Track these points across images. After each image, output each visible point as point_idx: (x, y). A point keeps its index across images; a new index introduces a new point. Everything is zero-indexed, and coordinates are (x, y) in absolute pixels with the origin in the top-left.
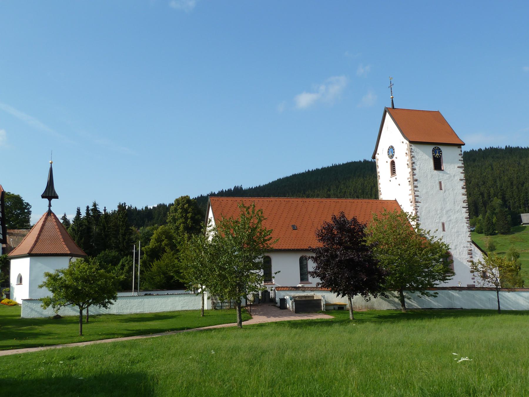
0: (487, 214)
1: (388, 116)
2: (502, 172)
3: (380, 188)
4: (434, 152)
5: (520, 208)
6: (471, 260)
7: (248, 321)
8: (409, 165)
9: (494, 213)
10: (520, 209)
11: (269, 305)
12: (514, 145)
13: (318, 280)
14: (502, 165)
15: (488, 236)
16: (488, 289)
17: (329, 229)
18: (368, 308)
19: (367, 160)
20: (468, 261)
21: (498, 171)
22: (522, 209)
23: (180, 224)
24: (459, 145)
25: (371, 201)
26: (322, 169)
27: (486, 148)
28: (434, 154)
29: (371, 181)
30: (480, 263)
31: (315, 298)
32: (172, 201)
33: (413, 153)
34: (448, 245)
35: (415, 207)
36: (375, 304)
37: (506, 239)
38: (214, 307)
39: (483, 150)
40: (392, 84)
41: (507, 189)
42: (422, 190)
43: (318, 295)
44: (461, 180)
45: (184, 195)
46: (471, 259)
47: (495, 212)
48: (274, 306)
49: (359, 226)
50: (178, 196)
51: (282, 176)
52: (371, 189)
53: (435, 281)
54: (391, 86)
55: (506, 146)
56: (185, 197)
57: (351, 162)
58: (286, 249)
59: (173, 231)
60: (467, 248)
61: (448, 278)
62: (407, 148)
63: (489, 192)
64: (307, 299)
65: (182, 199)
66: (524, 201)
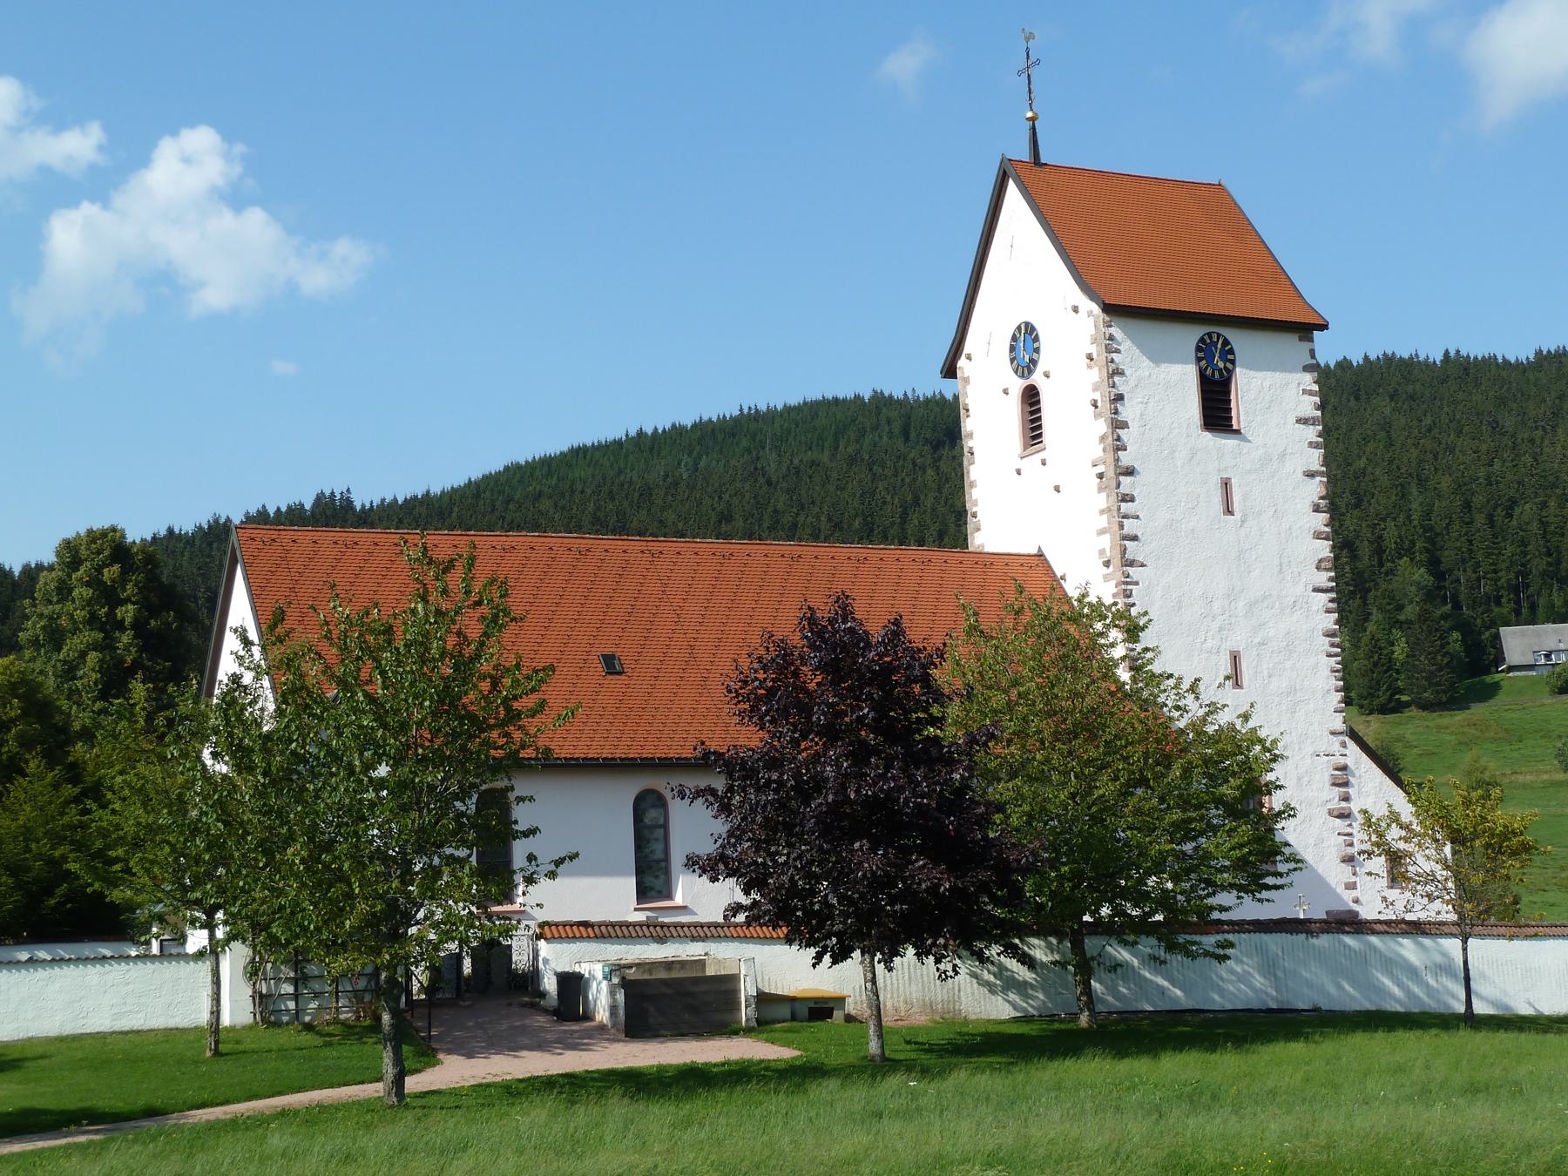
0: (1371, 627)
1: (1013, 195)
2: (1430, 457)
3: (975, 503)
4: (1201, 355)
5: (1498, 603)
6: (1343, 808)
7: (423, 1073)
8: (1099, 404)
9: (1397, 621)
10: (1497, 610)
11: (510, 1005)
12: (1475, 348)
13: (729, 891)
14: (1430, 430)
15: (1370, 718)
16: (1378, 927)
17: (783, 663)
18: (934, 1011)
19: (886, 395)
20: (1330, 812)
21: (1414, 453)
22: (1506, 608)
23: (83, 655)
24: (1306, 329)
25: (938, 555)
26: (695, 426)
27: (1366, 358)
28: (1203, 363)
29: (903, 480)
30: (1394, 818)
31: (710, 971)
32: (46, 554)
33: (1114, 356)
34: (1275, 742)
35: (1124, 583)
36: (962, 993)
37: (1439, 728)
38: (261, 1013)
39: (1355, 364)
40: (1033, 59)
41: (1448, 525)
42: (1150, 519)
43: (722, 956)
44: (1311, 475)
45: (100, 523)
46: (1344, 804)
47: (1402, 617)
48: (533, 1006)
49: (912, 658)
50: (76, 526)
51: (524, 452)
52: (900, 517)
53: (1214, 894)
54: (1028, 67)
55: (1447, 353)
56: (104, 534)
57: (820, 401)
58: (578, 758)
59: (51, 682)
60: (1327, 758)
61: (1270, 881)
62: (1094, 333)
63: (1380, 537)
64: (675, 974)
65: (94, 541)
66: (1512, 575)
